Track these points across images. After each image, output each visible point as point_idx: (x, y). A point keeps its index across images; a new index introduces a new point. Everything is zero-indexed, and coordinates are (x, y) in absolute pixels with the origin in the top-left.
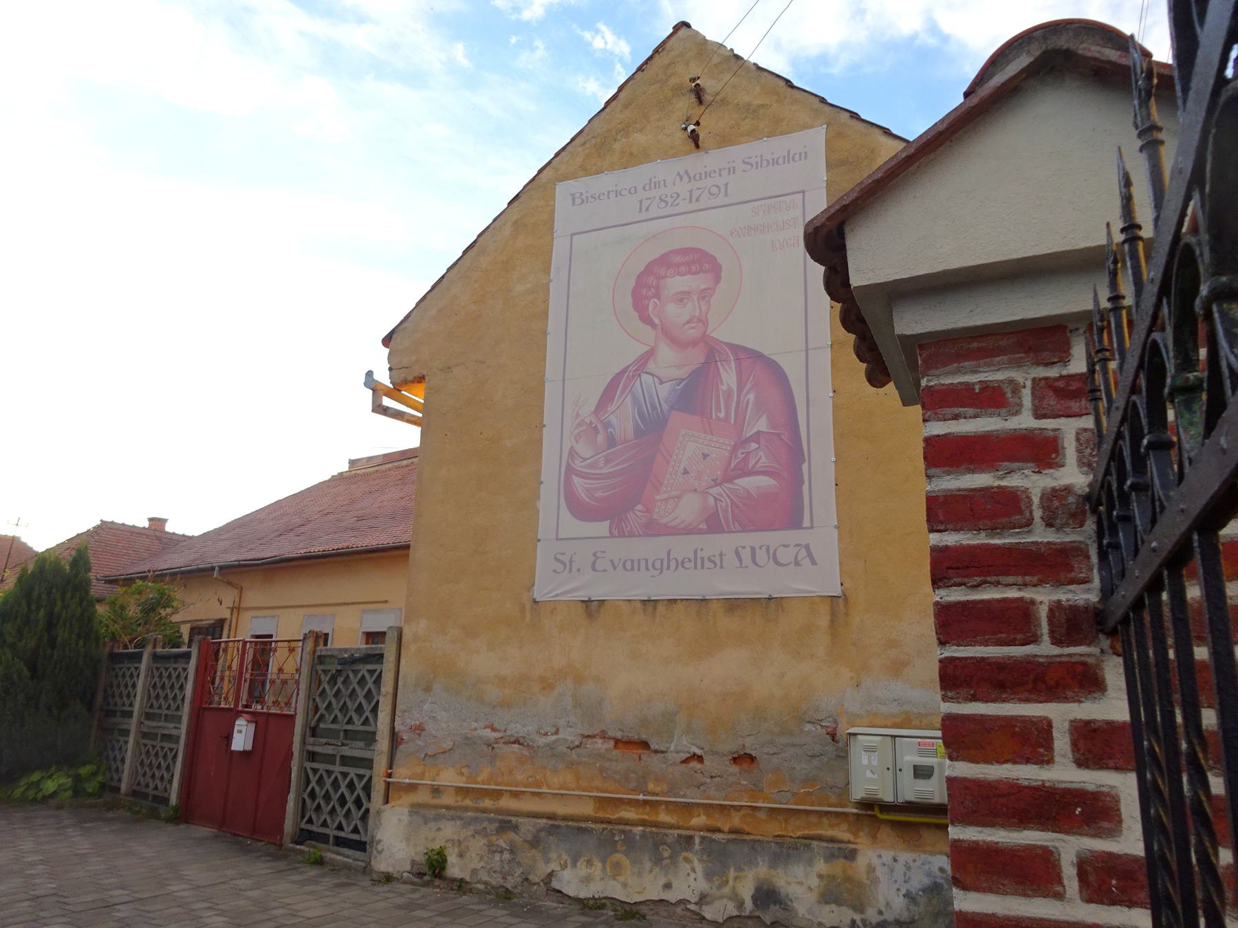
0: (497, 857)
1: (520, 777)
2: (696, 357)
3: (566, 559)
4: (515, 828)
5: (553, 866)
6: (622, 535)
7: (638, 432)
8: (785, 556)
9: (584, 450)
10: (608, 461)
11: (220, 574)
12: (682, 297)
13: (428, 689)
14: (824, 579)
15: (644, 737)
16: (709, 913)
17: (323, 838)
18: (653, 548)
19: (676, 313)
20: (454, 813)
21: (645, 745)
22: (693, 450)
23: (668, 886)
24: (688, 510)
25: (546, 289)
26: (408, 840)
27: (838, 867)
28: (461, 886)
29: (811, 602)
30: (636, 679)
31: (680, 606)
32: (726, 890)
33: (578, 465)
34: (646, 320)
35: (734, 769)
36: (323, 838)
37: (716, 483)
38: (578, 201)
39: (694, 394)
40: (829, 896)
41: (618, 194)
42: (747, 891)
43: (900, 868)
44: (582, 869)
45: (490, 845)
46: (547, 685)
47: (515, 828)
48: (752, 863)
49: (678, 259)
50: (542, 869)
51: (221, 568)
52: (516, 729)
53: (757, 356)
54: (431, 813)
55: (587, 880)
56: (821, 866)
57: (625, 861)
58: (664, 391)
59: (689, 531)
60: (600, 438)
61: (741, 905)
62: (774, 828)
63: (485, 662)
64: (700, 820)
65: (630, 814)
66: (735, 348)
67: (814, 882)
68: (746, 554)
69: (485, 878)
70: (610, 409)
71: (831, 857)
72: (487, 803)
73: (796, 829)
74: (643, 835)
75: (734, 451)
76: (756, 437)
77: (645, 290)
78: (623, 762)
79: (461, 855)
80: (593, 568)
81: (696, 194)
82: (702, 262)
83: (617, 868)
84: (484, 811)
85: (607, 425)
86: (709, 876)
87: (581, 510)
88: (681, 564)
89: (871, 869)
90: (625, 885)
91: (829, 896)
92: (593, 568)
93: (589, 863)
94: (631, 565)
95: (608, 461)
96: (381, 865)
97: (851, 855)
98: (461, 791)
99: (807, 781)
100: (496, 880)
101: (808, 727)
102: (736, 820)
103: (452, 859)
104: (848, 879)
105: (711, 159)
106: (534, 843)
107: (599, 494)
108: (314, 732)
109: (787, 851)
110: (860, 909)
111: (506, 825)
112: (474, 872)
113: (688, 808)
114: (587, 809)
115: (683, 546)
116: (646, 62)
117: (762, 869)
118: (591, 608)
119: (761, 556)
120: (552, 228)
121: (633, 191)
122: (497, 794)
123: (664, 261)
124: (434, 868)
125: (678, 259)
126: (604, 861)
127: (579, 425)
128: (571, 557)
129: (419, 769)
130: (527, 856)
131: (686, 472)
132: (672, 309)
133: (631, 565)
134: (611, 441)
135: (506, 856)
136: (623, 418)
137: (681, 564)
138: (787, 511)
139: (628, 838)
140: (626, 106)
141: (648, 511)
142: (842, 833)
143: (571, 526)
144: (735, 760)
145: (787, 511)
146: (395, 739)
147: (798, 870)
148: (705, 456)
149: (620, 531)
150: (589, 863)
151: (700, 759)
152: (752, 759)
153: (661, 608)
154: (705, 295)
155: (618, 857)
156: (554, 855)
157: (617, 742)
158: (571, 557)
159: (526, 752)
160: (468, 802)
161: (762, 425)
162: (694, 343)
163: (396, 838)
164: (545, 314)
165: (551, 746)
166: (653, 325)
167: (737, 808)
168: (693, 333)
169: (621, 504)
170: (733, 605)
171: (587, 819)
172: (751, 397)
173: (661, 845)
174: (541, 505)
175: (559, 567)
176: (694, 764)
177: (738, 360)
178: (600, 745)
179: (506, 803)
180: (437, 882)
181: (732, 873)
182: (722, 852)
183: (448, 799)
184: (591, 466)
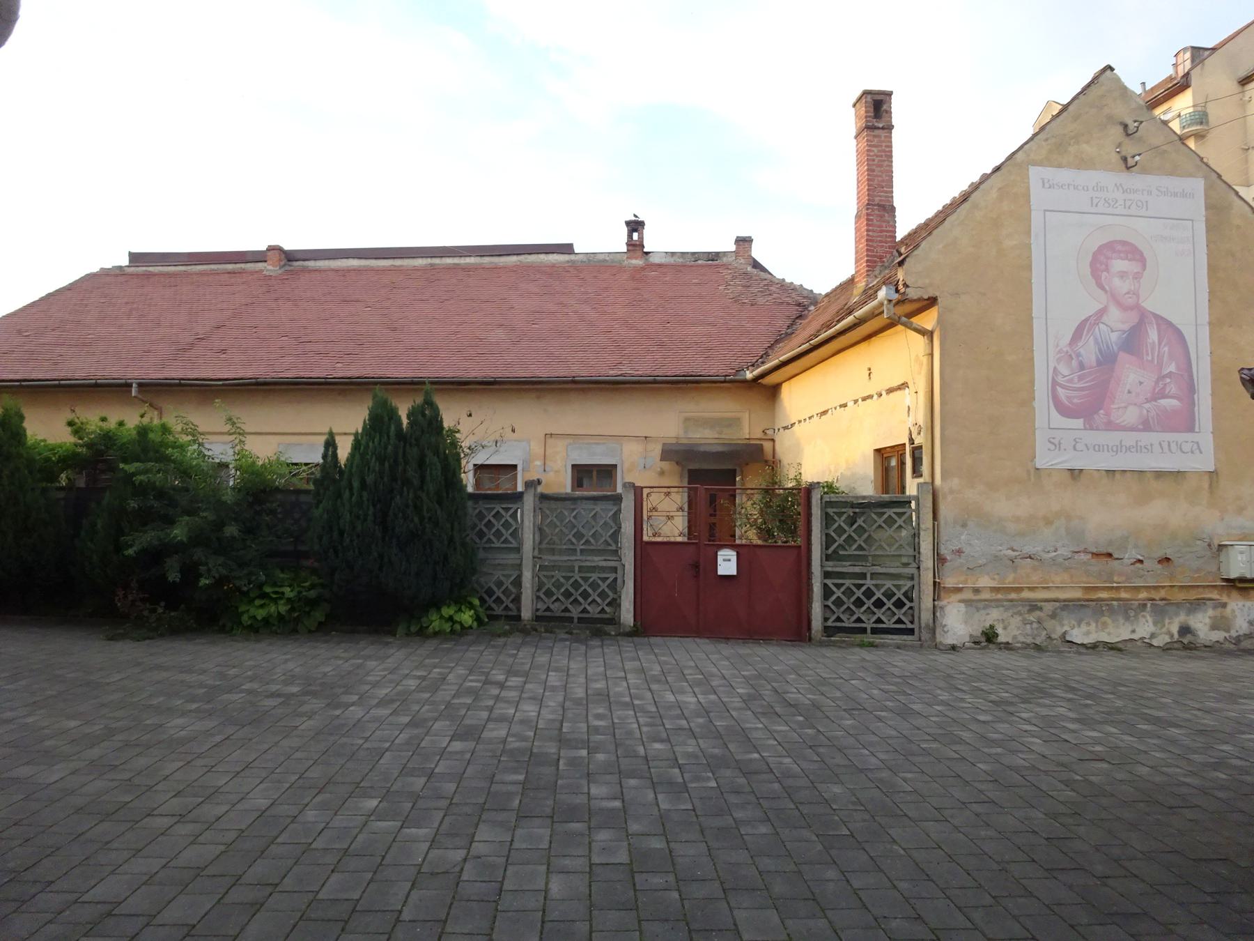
0: (1028, 627)
1: (1034, 578)
2: (1133, 318)
3: (1056, 441)
4: (1041, 609)
5: (1066, 628)
6: (1092, 429)
7: (1099, 363)
8: (1186, 447)
9: (1064, 370)
10: (1080, 378)
11: (139, 392)
12: (1123, 275)
13: (964, 525)
14: (1205, 462)
15: (1110, 551)
16: (1155, 643)
17: (864, 631)
18: (1113, 438)
19: (1121, 286)
20: (998, 603)
21: (1110, 555)
22: (1132, 378)
23: (1133, 631)
24: (1131, 416)
25: (1029, 246)
26: (966, 623)
27: (1219, 611)
28: (1007, 646)
29: (1200, 474)
30: (1105, 517)
31: (1128, 474)
32: (1164, 630)
33: (1060, 379)
34: (1102, 288)
35: (1159, 566)
36: (864, 631)
37: (1148, 401)
38: (1047, 185)
39: (1133, 341)
40: (1214, 627)
41: (1076, 188)
42: (1175, 629)
43: (1246, 609)
44: (1084, 628)
45: (1024, 619)
46: (1048, 522)
47: (1041, 609)
48: (1177, 614)
49: (1119, 247)
50: (1059, 631)
51: (140, 385)
52: (1028, 549)
53: (1170, 324)
54: (981, 605)
55: (1088, 633)
56: (1210, 612)
57: (1109, 621)
58: (1114, 336)
59: (1133, 429)
60: (1074, 363)
61: (1172, 636)
62: (1181, 596)
63: (1004, 507)
64: (1143, 595)
65: (1104, 595)
66: (1157, 316)
67: (1207, 621)
68: (1165, 445)
69: (1022, 639)
70: (1080, 344)
71: (1215, 608)
72: (1013, 596)
73: (1193, 595)
74: (1119, 606)
75: (1157, 382)
76: (1170, 375)
77: (1099, 262)
78: (1098, 565)
79: (1005, 628)
80: (1075, 449)
81: (1128, 203)
82: (1133, 252)
83: (1105, 625)
84: (1011, 601)
85: (1078, 355)
86: (1155, 623)
87: (1065, 411)
88: (1128, 449)
89: (1233, 611)
90: (1109, 634)
91: (1214, 627)
92: (1075, 449)
93: (1088, 624)
94: (1098, 448)
95: (1080, 378)
96: (949, 640)
97: (1224, 605)
98: (994, 589)
99: (1198, 570)
100: (1029, 640)
101: (1198, 542)
102: (1162, 593)
103: (1000, 631)
104: (1222, 617)
105: (1135, 181)
106: (1053, 616)
107: (1075, 401)
108: (828, 558)
109: (1196, 605)
110: (1228, 631)
111: (1034, 606)
112: (1015, 637)
113: (1137, 589)
114: (1078, 594)
115: (1129, 438)
116: (1089, 85)
117: (1182, 618)
118: (1075, 474)
119: (1173, 446)
120: (1028, 201)
121: (1086, 189)
122: (1019, 590)
123: (1110, 246)
124: (990, 636)
125: (1119, 247)
126: (1097, 622)
127: (1059, 352)
128: (1059, 442)
129: (962, 578)
130: (1049, 624)
131: (1129, 392)
132: (1117, 282)
133: (1098, 448)
134: (1082, 366)
135: (1035, 625)
136: (1089, 351)
137: (1128, 449)
138: (1188, 424)
139: (1111, 608)
140: (1076, 118)
141: (1108, 414)
142: (1215, 595)
143: (1058, 420)
144: (1160, 562)
145: (1188, 424)
146: (939, 559)
147: (1200, 616)
148: (1141, 383)
149: (1090, 426)
150: (1088, 624)
151: (1141, 561)
152: (1168, 559)
153: (1118, 476)
154: (1137, 276)
155: (1105, 619)
156: (1066, 622)
157: (1096, 555)
158: (1059, 442)
159: (1036, 563)
160: (1000, 596)
161: (1172, 368)
162: (1131, 308)
163: (957, 624)
164: (1029, 268)
165: (1053, 559)
166: (1106, 291)
167: (1163, 587)
168: (1130, 301)
169: (1090, 406)
170: (1159, 475)
171: (1079, 600)
172: (1166, 349)
173: (1128, 610)
174: (1036, 404)
175: (1052, 447)
176: (1138, 565)
177: (1158, 325)
178: (1083, 557)
179: (1026, 594)
180: (991, 646)
181: (1167, 621)
182: (1161, 609)
183: (985, 595)
184: (1069, 381)
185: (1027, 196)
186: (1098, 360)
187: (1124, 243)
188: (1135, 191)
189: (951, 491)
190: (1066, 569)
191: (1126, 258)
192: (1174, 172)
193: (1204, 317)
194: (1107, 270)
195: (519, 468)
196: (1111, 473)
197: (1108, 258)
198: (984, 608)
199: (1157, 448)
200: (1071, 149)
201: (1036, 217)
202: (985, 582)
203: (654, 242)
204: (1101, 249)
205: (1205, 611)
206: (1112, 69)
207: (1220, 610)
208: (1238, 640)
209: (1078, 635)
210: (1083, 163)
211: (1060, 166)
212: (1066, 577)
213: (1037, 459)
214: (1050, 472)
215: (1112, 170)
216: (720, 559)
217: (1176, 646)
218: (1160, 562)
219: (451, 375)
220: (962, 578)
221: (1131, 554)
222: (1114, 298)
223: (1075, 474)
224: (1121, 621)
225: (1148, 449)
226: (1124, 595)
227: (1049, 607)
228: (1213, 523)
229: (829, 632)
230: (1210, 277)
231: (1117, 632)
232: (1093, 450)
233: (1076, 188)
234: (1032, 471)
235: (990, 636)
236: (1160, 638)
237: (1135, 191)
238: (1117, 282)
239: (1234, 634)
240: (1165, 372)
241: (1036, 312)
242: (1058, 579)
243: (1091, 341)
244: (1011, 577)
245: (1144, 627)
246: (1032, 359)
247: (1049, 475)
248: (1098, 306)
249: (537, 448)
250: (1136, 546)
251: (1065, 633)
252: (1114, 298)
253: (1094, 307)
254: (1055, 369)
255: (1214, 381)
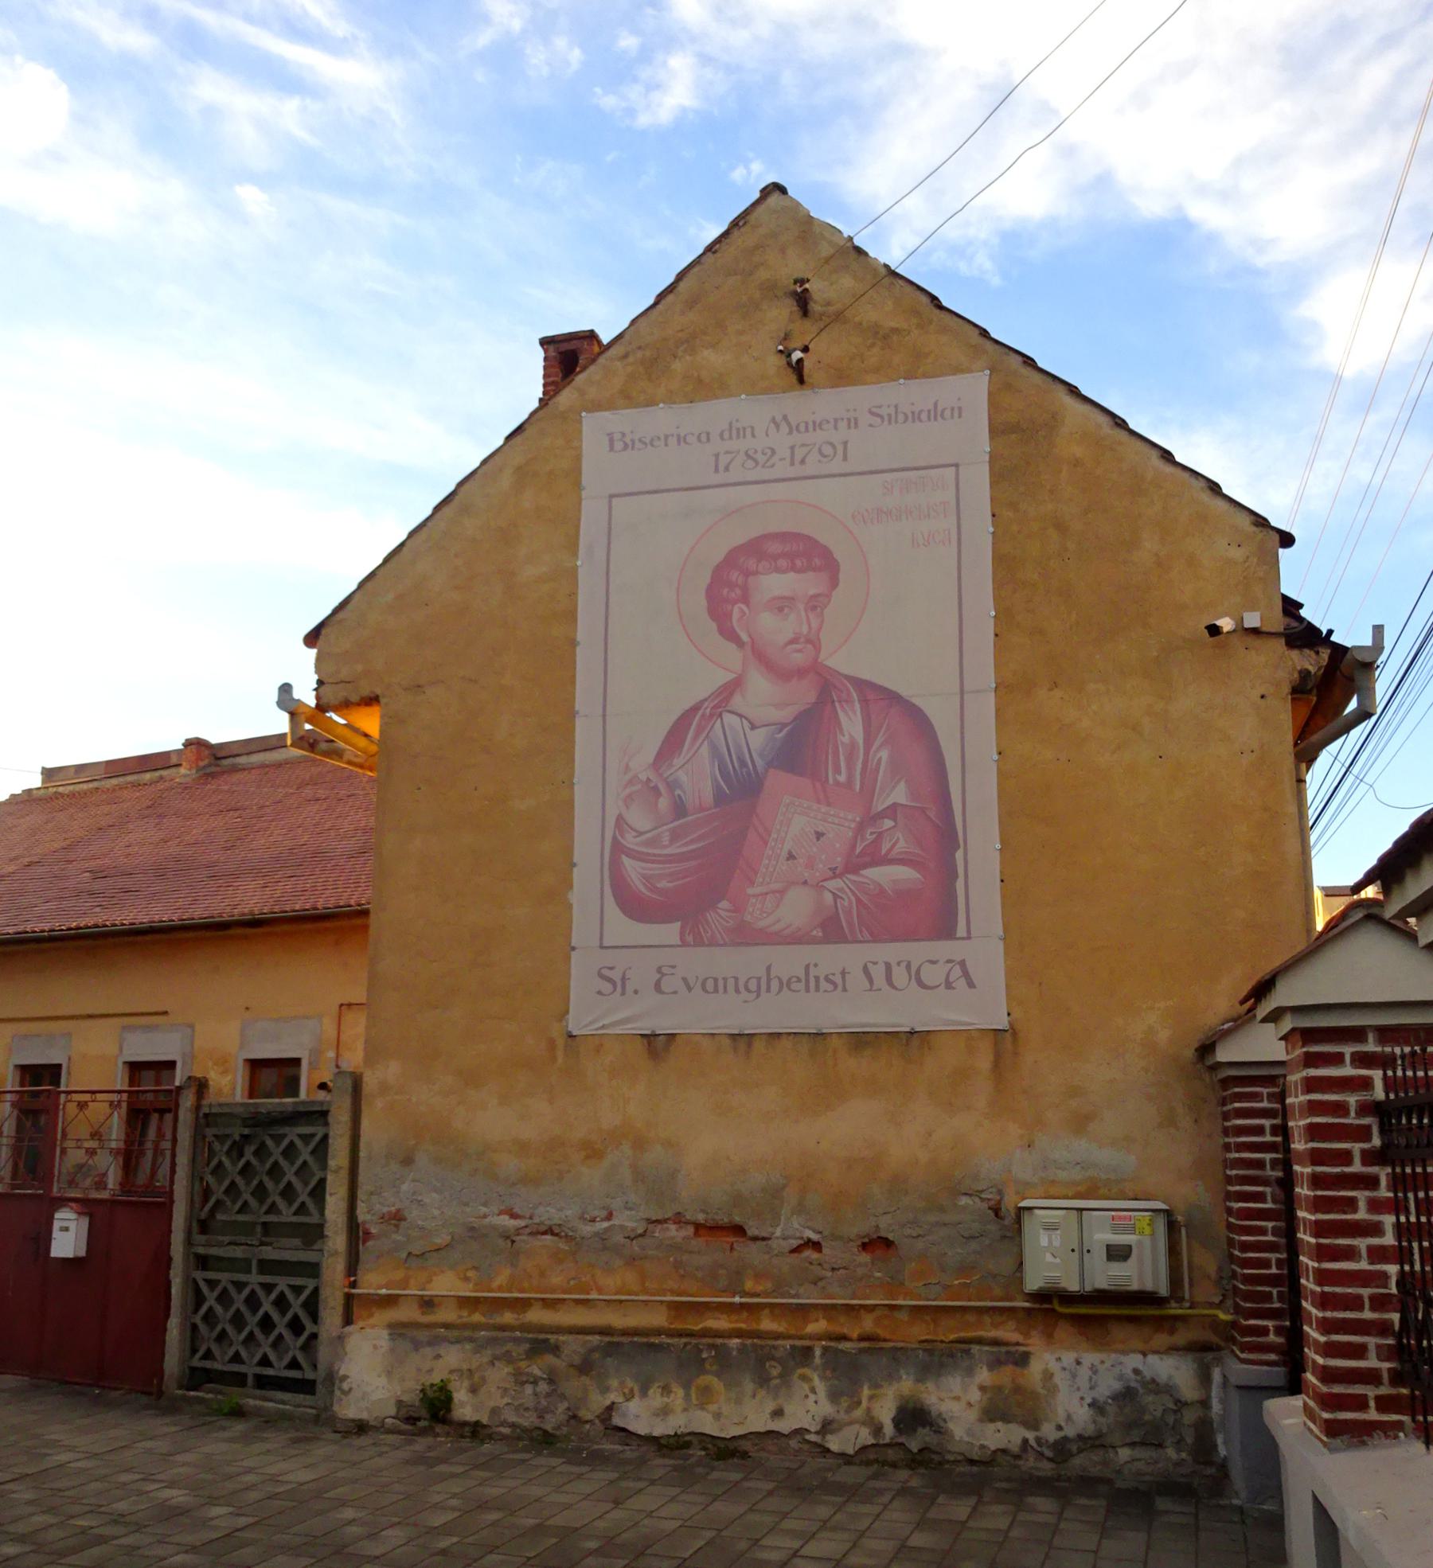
1: (556, 1280)
2: (805, 693)
3: (616, 975)
4: (555, 1349)
5: (613, 1397)
6: (699, 942)
7: (720, 798)
9: (639, 819)
10: (675, 836)
12: (782, 605)
13: (408, 1161)
14: (986, 1006)
15: (737, 1219)
16: (834, 1444)
17: (239, 1380)
18: (748, 961)
19: (774, 629)
21: (739, 1230)
22: (800, 826)
23: (778, 1413)
25: (573, 573)
26: (389, 1374)
28: (475, 1431)
29: (969, 1037)
30: (720, 1142)
31: (786, 1043)
32: (859, 1413)
33: (630, 841)
35: (865, 1258)
36: (239, 1380)
37: (835, 874)
38: (619, 445)
39: (802, 746)
40: (993, 1413)
42: (886, 1412)
43: (1084, 1372)
44: (656, 1399)
46: (592, 1152)
47: (555, 1349)
48: (892, 1377)
49: (774, 548)
50: (597, 1402)
52: (549, 1214)
53: (892, 698)
54: (422, 1335)
56: (984, 1375)
58: (757, 739)
59: (796, 939)
60: (664, 803)
61: (878, 1430)
62: (919, 1331)
63: (496, 1121)
65: (721, 1323)
66: (862, 685)
67: (975, 1395)
68: (878, 973)
70: (678, 762)
71: (995, 1364)
72: (508, 1317)
73: (949, 1331)
74: (742, 1349)
75: (860, 829)
76: (892, 811)
77: (726, 589)
78: (707, 1254)
79: (474, 1390)
81: (800, 453)
82: (809, 554)
84: (502, 1328)
85: (672, 786)
86: (834, 1396)
87: (635, 906)
88: (786, 985)
89: (1048, 1376)
91: (993, 1413)
92: (658, 987)
93: (666, 1390)
94: (714, 986)
96: (349, 1409)
97: (1023, 1360)
98: (464, 1302)
99: (964, 1269)
100: (528, 1420)
101: (964, 1201)
102: (868, 1324)
103: (460, 1395)
104: (1018, 1390)
105: (822, 403)
106: (585, 1367)
107: (663, 884)
110: (1033, 1424)
111: (541, 1344)
112: (495, 1411)
113: (803, 1312)
114: (658, 1319)
115: (788, 961)
119: (900, 976)
120: (577, 485)
121: (705, 438)
122: (524, 1304)
123: (755, 548)
125: (774, 548)
126: (686, 1386)
127: (630, 782)
129: (399, 1275)
130: (573, 1386)
132: (767, 622)
133: (714, 986)
134: (679, 809)
135: (543, 1387)
136: (697, 775)
137: (786, 985)
138: (942, 922)
140: (692, 303)
141: (738, 909)
142: (1008, 1332)
143: (622, 928)
145: (942, 922)
146: (356, 1233)
147: (953, 1382)
148: (819, 835)
149: (695, 937)
150: (666, 1390)
151: (817, 1246)
152: (887, 1243)
153: (759, 1046)
154: (816, 604)
158: (621, 974)
159: (563, 1245)
160: (477, 1317)
161: (900, 795)
162: (801, 673)
163: (369, 1371)
164: (571, 616)
168: (799, 659)
169: (697, 892)
170: (861, 1041)
171: (658, 1332)
172: (884, 754)
173: (766, 1362)
174: (574, 897)
175: (607, 987)
176: (808, 1253)
177: (864, 702)
180: (439, 1429)
181: (866, 1392)
184: (651, 843)
185: (574, 475)
186: (717, 789)
187: (783, 537)
188: (817, 426)
189: (384, 1088)
190: (632, 1261)
191: (793, 568)
192: (917, 368)
193: (984, 672)
194: (745, 599)
195: (305, 1064)
196: (742, 1040)
197: (747, 574)
198: (430, 1344)
199: (856, 978)
200: (677, 366)
201: (592, 512)
202: (446, 1284)
203: (1333, 638)
204: (731, 560)
205: (970, 1372)
206: (782, 190)
207: (1008, 1370)
208: (1061, 1449)
209: (642, 1415)
210: (702, 388)
211: (651, 403)
212: (630, 1278)
213: (570, 1016)
214: (598, 1043)
215: (768, 391)
216: (56, 1225)
217: (891, 1455)
218: (865, 1247)
219: (332, 903)
220: (399, 1275)
221: (793, 1227)
222: (761, 657)
223: (656, 1045)
224: (749, 1386)
225: (837, 983)
226: (767, 1324)
227: (573, 1346)
228: (997, 1150)
229: (197, 1378)
230: (998, 585)
231: (740, 1412)
232: (700, 990)
233: (681, 440)
234: (560, 1042)
235: (434, 1409)
236: (849, 1432)
237: (817, 426)
238: (767, 622)
239: (1049, 1432)
240: (880, 805)
241: (585, 697)
242: (614, 1280)
243: (705, 750)
244: (501, 1279)
245: (807, 1405)
246: (570, 804)
247: (598, 1049)
248: (722, 677)
249: (329, 1028)
250: (800, 1209)
251: (611, 1408)
252: (761, 657)
253: (707, 681)
254: (620, 819)
255: (1007, 816)
